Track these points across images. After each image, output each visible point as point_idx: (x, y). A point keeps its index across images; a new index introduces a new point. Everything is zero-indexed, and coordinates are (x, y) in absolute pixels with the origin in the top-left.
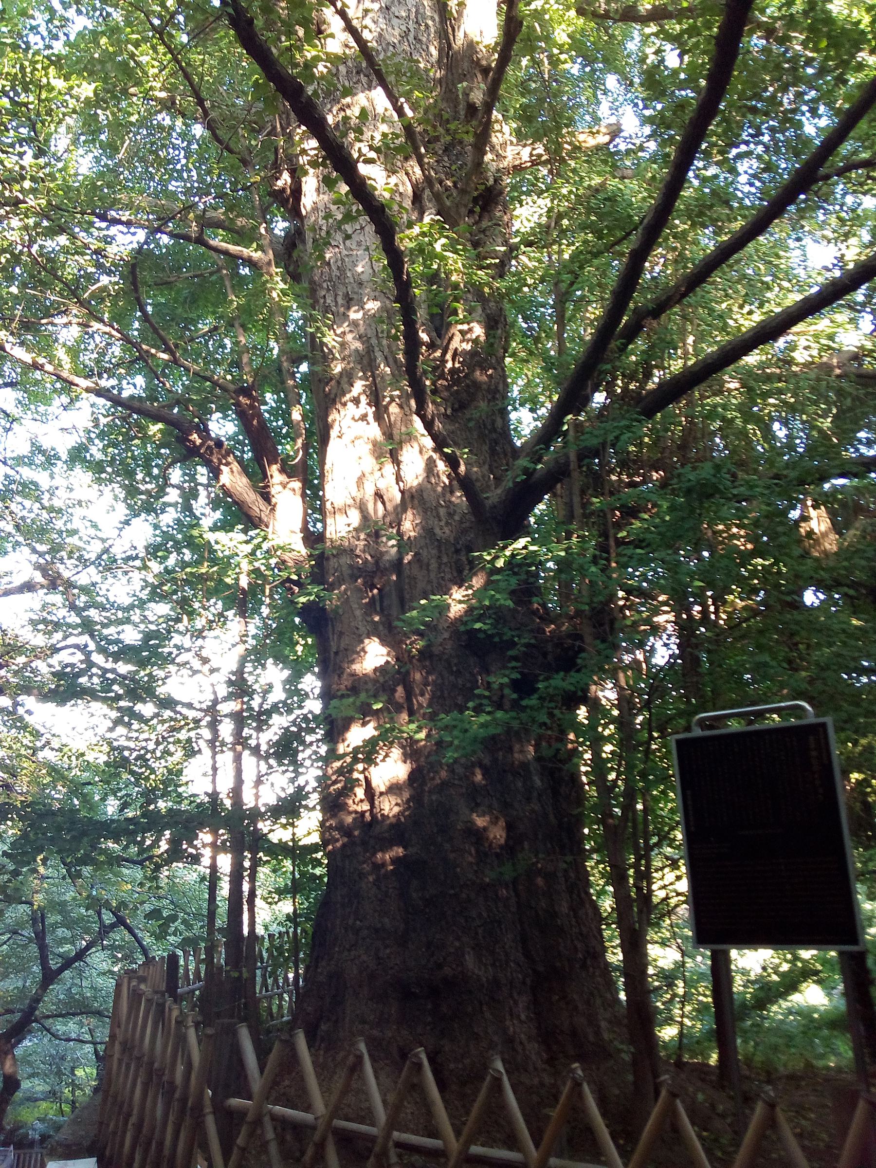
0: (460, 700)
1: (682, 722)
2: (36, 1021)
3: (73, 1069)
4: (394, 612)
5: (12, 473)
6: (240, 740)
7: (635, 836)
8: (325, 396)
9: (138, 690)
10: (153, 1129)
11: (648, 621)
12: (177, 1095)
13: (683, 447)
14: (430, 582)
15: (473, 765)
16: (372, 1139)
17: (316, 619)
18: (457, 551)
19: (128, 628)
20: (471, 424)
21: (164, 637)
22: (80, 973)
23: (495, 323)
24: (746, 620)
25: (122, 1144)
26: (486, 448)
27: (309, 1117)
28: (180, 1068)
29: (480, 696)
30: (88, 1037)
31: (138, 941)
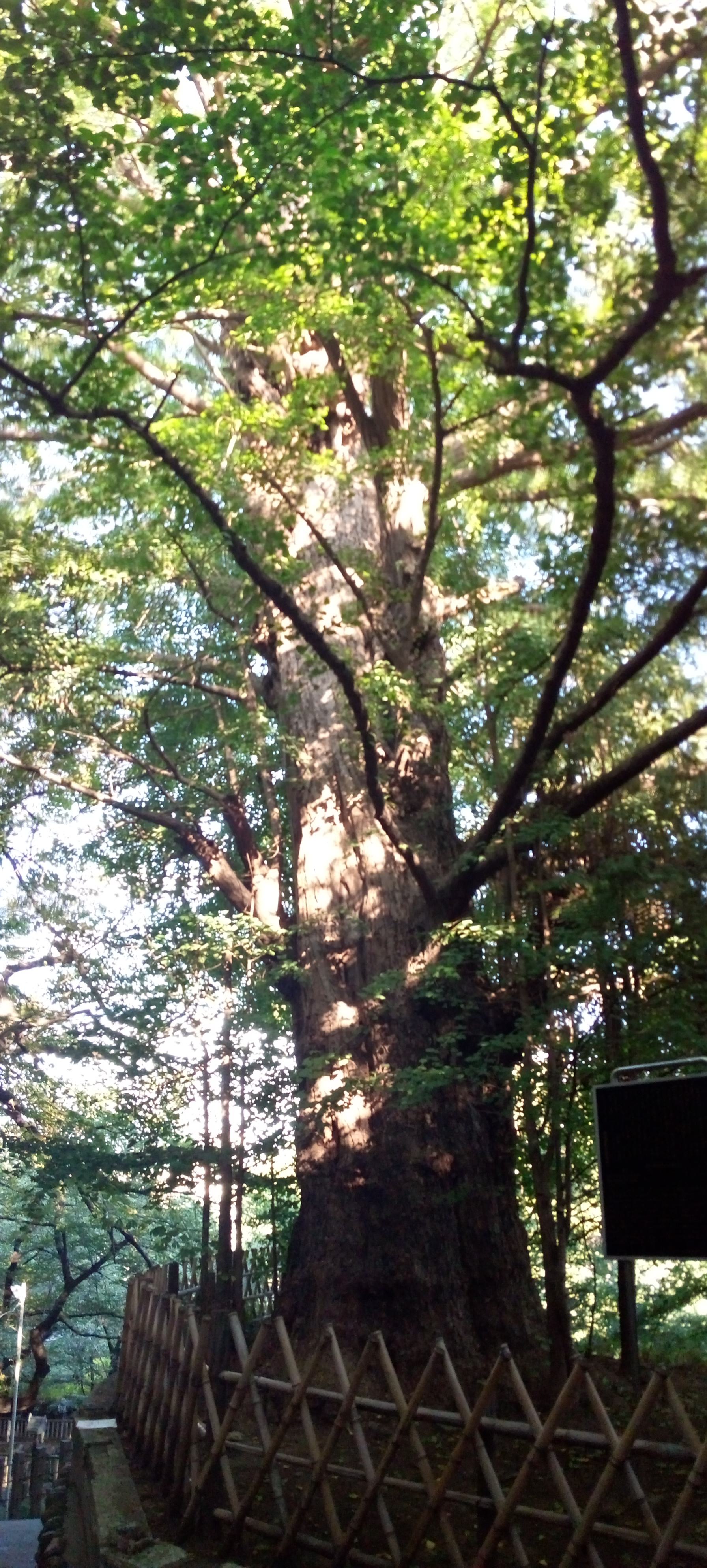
0: (413, 1058)
1: (603, 1077)
2: (61, 1320)
3: (91, 1359)
4: (358, 983)
5: (35, 867)
6: (227, 1092)
7: (558, 1172)
8: (298, 795)
9: (139, 1050)
10: (161, 1396)
11: (577, 992)
12: (181, 1369)
13: (606, 841)
14: (388, 957)
15: (424, 1112)
16: (338, 1403)
17: (291, 989)
18: (411, 931)
19: (131, 996)
20: (422, 824)
21: (161, 1004)
22: (96, 1282)
23: (438, 737)
24: (663, 991)
25: (136, 1409)
26: (435, 843)
27: (287, 1386)
28: (182, 1350)
29: (430, 1054)
30: (103, 1334)
31: (144, 1256)
